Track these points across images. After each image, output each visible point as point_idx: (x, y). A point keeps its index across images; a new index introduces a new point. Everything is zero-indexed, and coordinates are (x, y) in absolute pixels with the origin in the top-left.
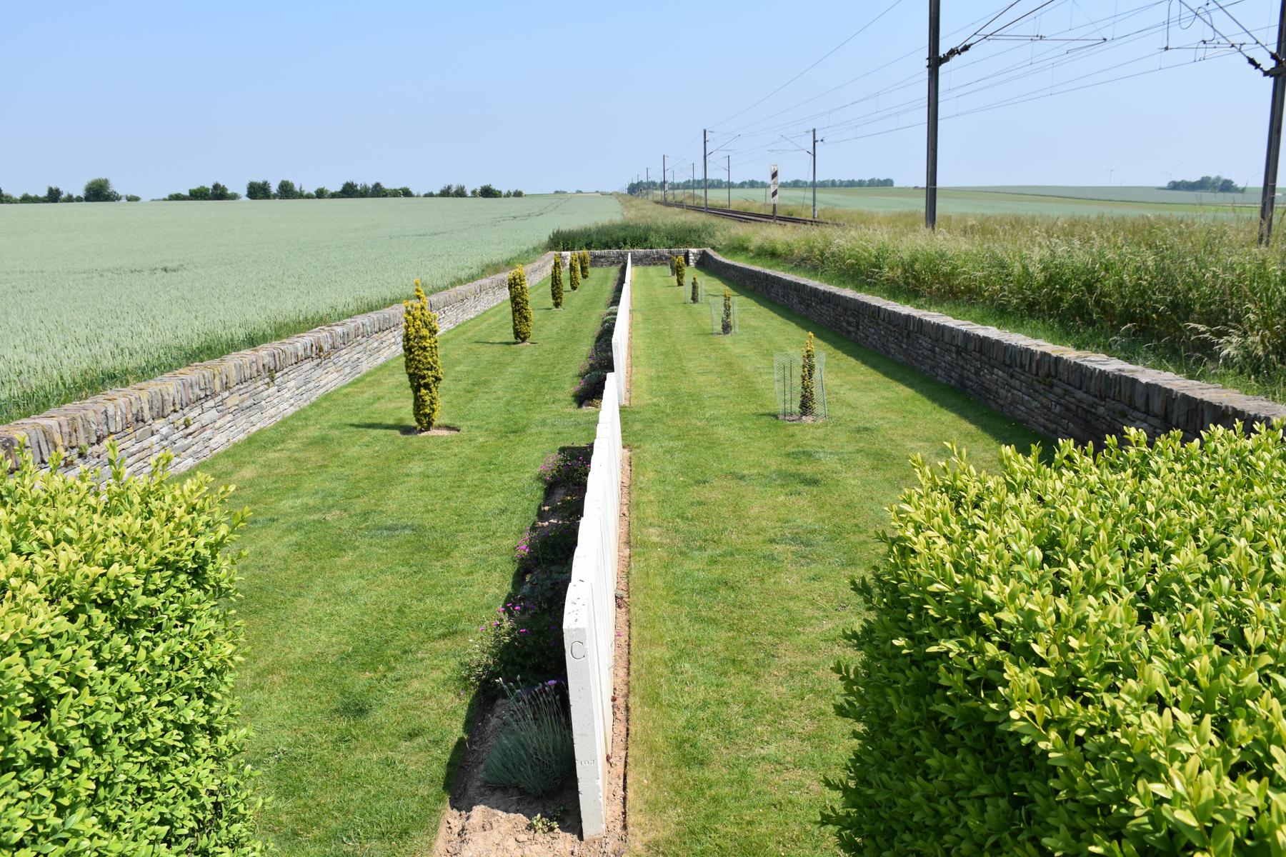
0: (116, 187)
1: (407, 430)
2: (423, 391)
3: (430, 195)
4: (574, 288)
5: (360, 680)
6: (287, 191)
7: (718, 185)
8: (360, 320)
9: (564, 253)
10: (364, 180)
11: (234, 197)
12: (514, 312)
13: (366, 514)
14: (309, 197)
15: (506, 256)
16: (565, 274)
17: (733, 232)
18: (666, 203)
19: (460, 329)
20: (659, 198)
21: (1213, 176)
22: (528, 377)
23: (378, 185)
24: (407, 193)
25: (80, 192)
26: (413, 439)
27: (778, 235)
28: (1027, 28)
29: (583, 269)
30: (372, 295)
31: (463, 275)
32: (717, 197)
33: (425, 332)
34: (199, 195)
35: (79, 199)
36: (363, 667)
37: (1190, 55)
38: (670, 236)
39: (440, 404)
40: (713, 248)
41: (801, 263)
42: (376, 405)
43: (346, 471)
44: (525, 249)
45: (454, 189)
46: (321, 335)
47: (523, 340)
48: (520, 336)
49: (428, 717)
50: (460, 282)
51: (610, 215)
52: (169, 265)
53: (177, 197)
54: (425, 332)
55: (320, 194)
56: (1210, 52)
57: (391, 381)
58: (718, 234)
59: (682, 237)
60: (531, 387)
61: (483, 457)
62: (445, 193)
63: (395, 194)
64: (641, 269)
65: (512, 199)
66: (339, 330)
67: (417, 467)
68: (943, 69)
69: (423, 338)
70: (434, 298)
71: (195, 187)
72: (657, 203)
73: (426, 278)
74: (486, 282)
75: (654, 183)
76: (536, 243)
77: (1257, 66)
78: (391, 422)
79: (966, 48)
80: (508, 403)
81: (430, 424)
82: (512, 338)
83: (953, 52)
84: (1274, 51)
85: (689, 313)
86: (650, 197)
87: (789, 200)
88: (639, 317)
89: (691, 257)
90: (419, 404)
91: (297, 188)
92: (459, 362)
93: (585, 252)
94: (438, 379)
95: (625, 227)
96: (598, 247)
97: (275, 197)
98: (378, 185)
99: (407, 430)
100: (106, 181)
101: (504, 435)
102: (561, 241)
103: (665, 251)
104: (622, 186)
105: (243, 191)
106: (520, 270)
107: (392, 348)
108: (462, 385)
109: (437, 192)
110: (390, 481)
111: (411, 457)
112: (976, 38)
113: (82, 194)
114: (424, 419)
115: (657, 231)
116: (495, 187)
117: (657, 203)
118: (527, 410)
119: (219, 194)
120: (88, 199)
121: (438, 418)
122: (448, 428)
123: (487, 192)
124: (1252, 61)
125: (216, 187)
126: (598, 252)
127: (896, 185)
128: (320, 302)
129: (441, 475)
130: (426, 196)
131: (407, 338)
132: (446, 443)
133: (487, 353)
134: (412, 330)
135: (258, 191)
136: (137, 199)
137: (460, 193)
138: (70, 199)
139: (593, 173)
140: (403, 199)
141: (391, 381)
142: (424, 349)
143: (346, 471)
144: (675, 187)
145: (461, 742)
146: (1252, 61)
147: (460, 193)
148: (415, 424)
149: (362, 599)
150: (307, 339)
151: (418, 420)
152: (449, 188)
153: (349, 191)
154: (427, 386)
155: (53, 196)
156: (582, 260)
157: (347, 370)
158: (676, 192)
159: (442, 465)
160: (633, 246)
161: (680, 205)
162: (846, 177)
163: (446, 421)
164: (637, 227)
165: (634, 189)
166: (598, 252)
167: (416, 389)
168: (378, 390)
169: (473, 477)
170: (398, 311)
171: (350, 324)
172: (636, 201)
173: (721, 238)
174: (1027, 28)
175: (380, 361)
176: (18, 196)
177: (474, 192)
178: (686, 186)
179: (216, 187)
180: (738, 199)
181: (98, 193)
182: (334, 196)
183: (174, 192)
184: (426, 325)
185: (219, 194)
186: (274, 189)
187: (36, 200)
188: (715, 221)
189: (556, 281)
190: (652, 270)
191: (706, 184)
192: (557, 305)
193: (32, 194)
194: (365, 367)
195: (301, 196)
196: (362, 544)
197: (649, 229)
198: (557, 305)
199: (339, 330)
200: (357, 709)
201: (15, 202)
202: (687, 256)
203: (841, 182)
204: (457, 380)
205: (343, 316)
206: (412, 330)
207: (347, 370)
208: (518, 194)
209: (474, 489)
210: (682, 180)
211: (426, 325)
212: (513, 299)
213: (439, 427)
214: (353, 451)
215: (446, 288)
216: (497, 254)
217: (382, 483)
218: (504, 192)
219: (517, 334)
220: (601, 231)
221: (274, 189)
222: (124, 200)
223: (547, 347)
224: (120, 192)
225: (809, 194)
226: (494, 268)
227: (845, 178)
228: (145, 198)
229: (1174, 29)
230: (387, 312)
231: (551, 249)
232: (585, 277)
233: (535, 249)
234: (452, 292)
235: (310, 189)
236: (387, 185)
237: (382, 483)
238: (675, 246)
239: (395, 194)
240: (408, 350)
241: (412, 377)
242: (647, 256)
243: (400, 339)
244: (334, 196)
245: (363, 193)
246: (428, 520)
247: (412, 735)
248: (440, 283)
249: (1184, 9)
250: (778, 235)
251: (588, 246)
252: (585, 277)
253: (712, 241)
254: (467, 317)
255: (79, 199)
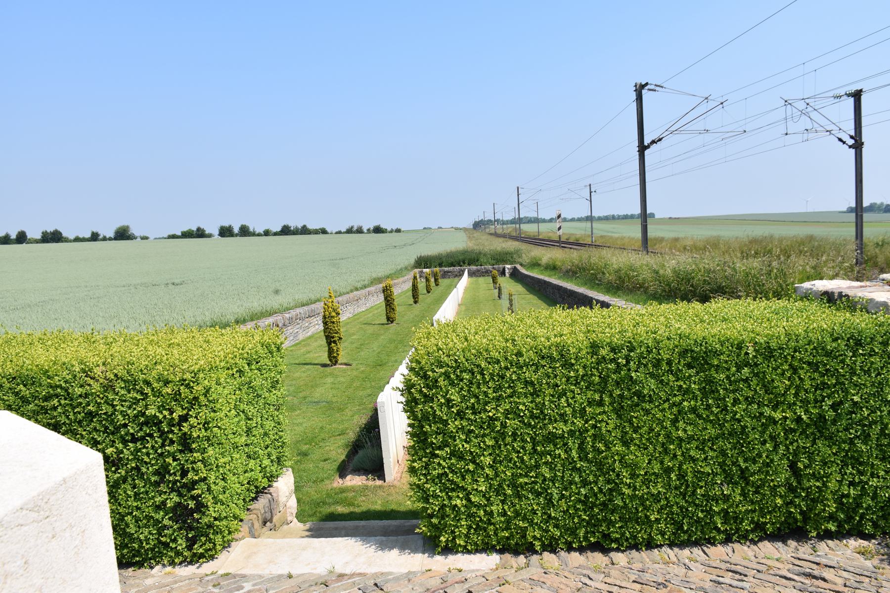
0: (134, 230)
1: (324, 365)
2: (333, 345)
3: (339, 232)
4: (429, 292)
5: (305, 448)
6: (245, 232)
7: (530, 221)
8: (298, 310)
9: (425, 270)
10: (293, 224)
11: (210, 236)
12: (386, 305)
13: (305, 398)
14: (259, 235)
15: (388, 272)
16: (422, 284)
17: (533, 254)
18: (496, 235)
19: (356, 317)
20: (493, 231)
21: (878, 202)
22: (391, 341)
23: (305, 226)
24: (324, 231)
25: (111, 234)
26: (328, 369)
27: (546, 255)
28: (699, 125)
29: (436, 280)
30: (303, 297)
31: (359, 285)
32: (529, 229)
33: (334, 314)
34: (187, 235)
35: (110, 239)
36: (306, 444)
37: (799, 138)
38: (493, 258)
39: (341, 353)
40: (521, 265)
41: (572, 273)
42: (308, 355)
43: (294, 382)
44: (399, 267)
45: (355, 229)
46: (278, 318)
47: (392, 322)
48: (390, 320)
49: (333, 455)
50: (357, 289)
51: (458, 244)
52: (176, 281)
53: (173, 237)
54: (334, 314)
55: (267, 233)
56: (811, 135)
57: (315, 344)
58: (524, 255)
59: (501, 258)
60: (393, 345)
61: (364, 376)
62: (350, 231)
63: (316, 232)
64: (474, 279)
65: (394, 233)
66: (287, 316)
67: (329, 380)
68: (647, 152)
69: (333, 317)
70: (340, 299)
71: (185, 229)
72: (491, 234)
73: (336, 287)
74: (372, 289)
75: (490, 221)
76: (406, 263)
77: (844, 143)
78: (316, 362)
79: (660, 140)
80: (379, 353)
81: (336, 362)
82: (385, 321)
83: (653, 142)
84: (853, 133)
85: (495, 305)
86: (487, 230)
87: (569, 230)
88: (463, 308)
89: (507, 271)
90: (330, 351)
91: (251, 230)
92: (354, 334)
93: (438, 269)
94: (340, 338)
95: (464, 252)
96: (442, 267)
97: (237, 235)
98: (305, 226)
99: (324, 365)
100: (128, 227)
101: (375, 367)
102: (422, 262)
103: (490, 267)
104: (468, 224)
105: (216, 232)
106: (390, 282)
107: (317, 326)
108: (355, 345)
109: (344, 230)
110: (317, 386)
111: (326, 376)
112: (667, 133)
113: (112, 235)
114: (333, 359)
115: (485, 255)
116: (383, 226)
117: (491, 234)
118: (388, 356)
119: (200, 234)
120: (116, 239)
121: (341, 360)
122: (346, 364)
123: (378, 230)
124: (840, 140)
125: (199, 229)
126: (446, 269)
127: (656, 217)
128: (275, 302)
129: (340, 383)
130: (337, 233)
131: (324, 317)
132: (344, 371)
133: (370, 329)
134: (327, 313)
135: (226, 232)
136: (147, 238)
137: (360, 231)
138: (105, 239)
139: (447, 216)
140: (321, 236)
141: (315, 344)
142: (333, 323)
143: (294, 382)
144: (504, 223)
145: (344, 461)
146: (840, 140)
147: (360, 231)
148: (329, 362)
149: (304, 425)
150: (270, 320)
151: (330, 360)
152: (352, 227)
153: (286, 231)
154: (335, 342)
155: (95, 237)
156: (435, 275)
157: (292, 338)
158: (505, 226)
159: (342, 379)
160: (469, 265)
161: (504, 236)
162: (622, 213)
163: (345, 361)
164: (472, 251)
165: (477, 225)
166: (446, 269)
167: (329, 344)
168: (308, 348)
169: (357, 384)
170: (319, 306)
171: (293, 313)
172: (476, 234)
173: (525, 259)
174: (699, 125)
175: (309, 334)
176: (72, 237)
177: (368, 230)
178: (513, 222)
179: (199, 229)
180: (545, 230)
181: (123, 234)
182: (276, 234)
183: (172, 233)
184: (334, 310)
185: (200, 234)
186: (236, 230)
187: (83, 240)
188: (523, 247)
189: (415, 288)
190: (481, 280)
191: (519, 221)
192: (416, 302)
193: (81, 236)
194: (301, 337)
195: (254, 234)
196: (304, 408)
197: (480, 253)
198: (416, 302)
199: (287, 316)
200: (305, 454)
201: (70, 241)
202: (504, 269)
203: (619, 216)
204: (352, 343)
205: (288, 309)
206: (327, 313)
207: (292, 338)
208: (398, 231)
209: (357, 388)
210: (510, 218)
211: (334, 310)
212: (386, 299)
213: (341, 364)
214: (297, 375)
215: (348, 293)
216: (381, 272)
217: (312, 387)
218: (389, 229)
219: (388, 319)
220: (450, 255)
221: (236, 230)
222: (139, 239)
223: (405, 325)
224: (137, 234)
225: (589, 224)
226: (379, 280)
227: (622, 213)
228: (152, 237)
229: (790, 123)
230: (313, 306)
231: (416, 268)
232: (437, 285)
233: (406, 268)
234: (351, 295)
235: (260, 230)
236: (311, 226)
237: (312, 387)
238: (496, 264)
239: (316, 232)
240: (325, 323)
241: (327, 337)
242: (478, 271)
243: (320, 322)
244: (276, 234)
245: (296, 232)
246: (334, 400)
247: (325, 460)
248: (344, 291)
249: (795, 110)
250: (546, 255)
251: (440, 265)
252: (437, 285)
253: (520, 260)
254: (360, 310)
255: (110, 239)
